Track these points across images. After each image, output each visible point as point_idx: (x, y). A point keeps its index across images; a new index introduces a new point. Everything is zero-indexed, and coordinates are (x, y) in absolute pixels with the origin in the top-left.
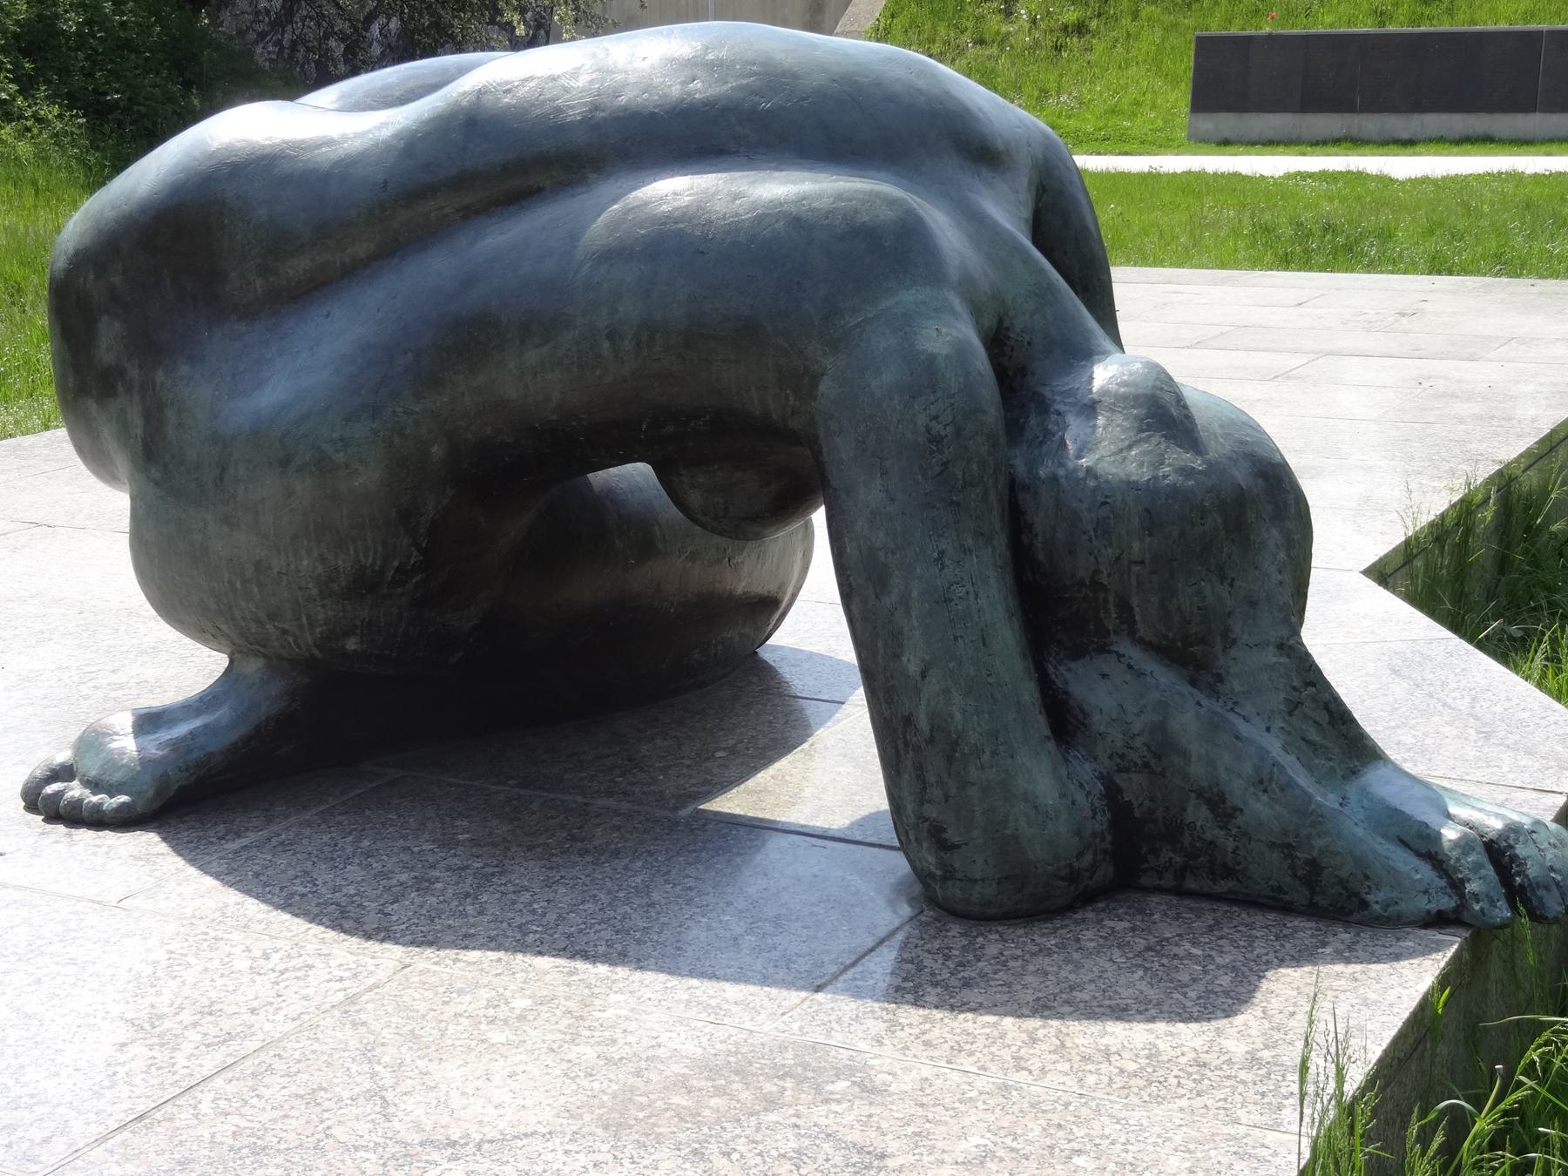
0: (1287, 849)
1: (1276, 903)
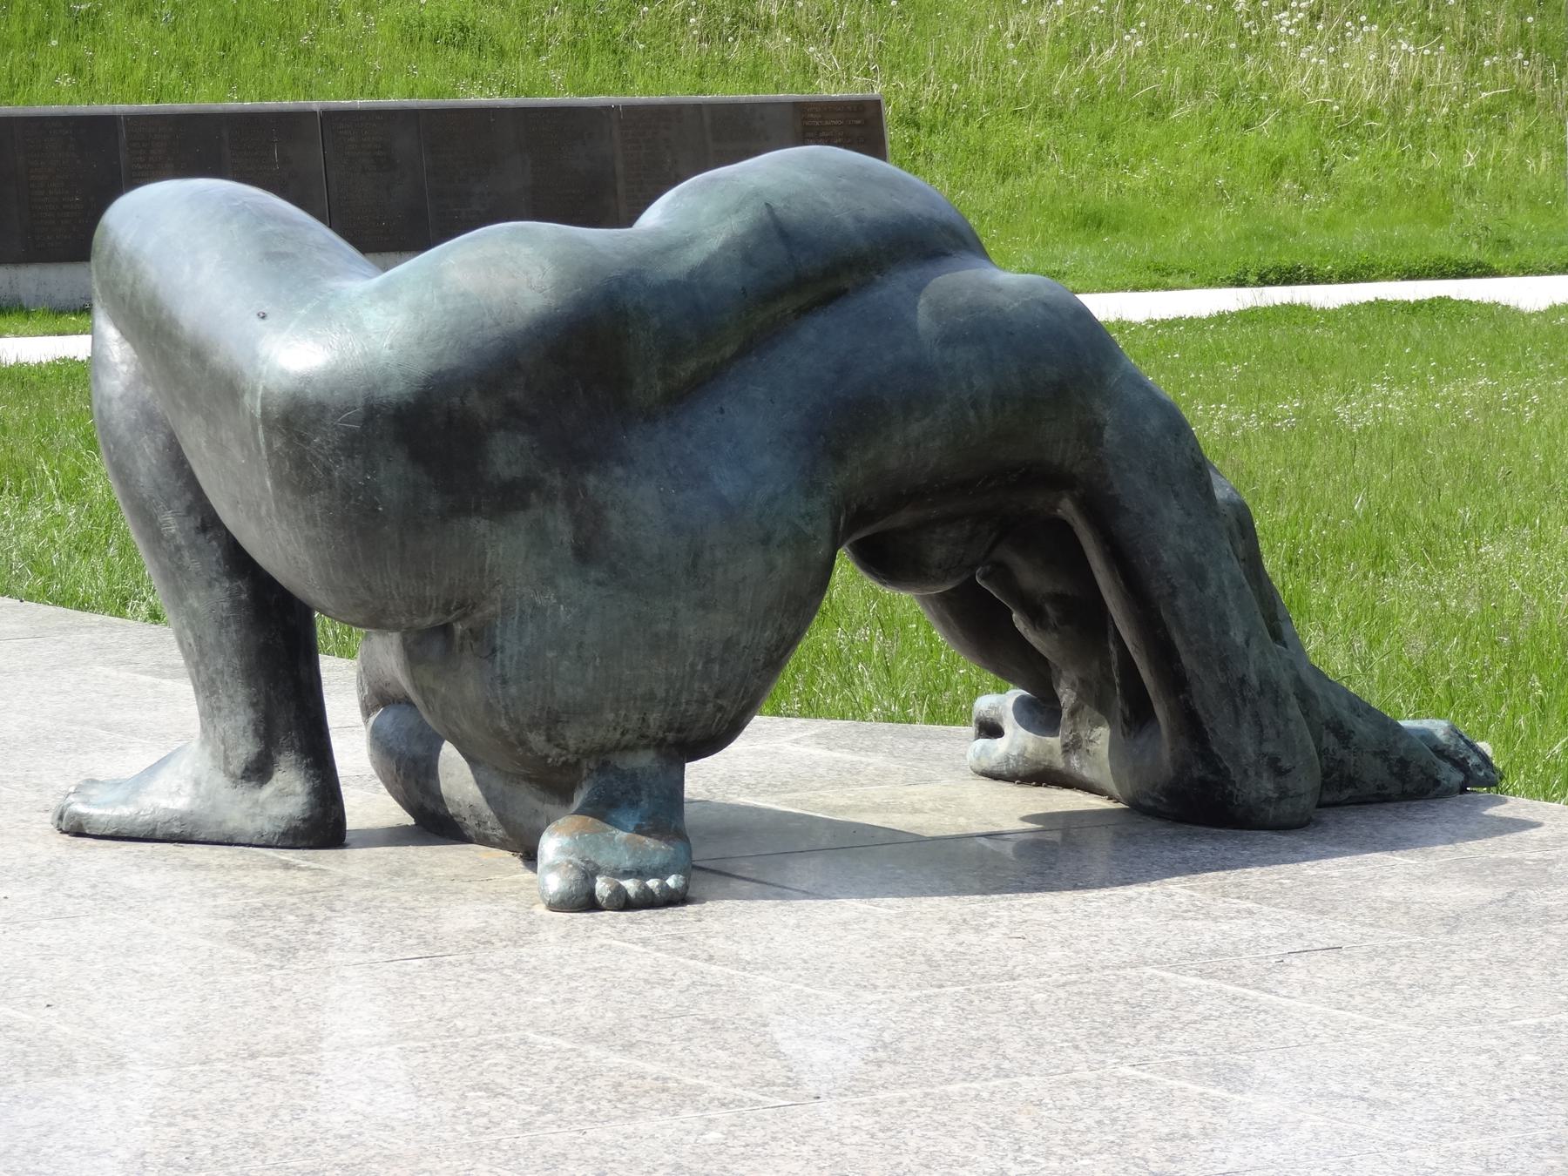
0: (1383, 755)
1: (1379, 798)
